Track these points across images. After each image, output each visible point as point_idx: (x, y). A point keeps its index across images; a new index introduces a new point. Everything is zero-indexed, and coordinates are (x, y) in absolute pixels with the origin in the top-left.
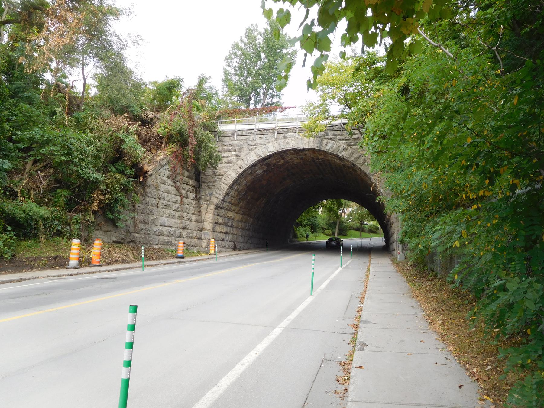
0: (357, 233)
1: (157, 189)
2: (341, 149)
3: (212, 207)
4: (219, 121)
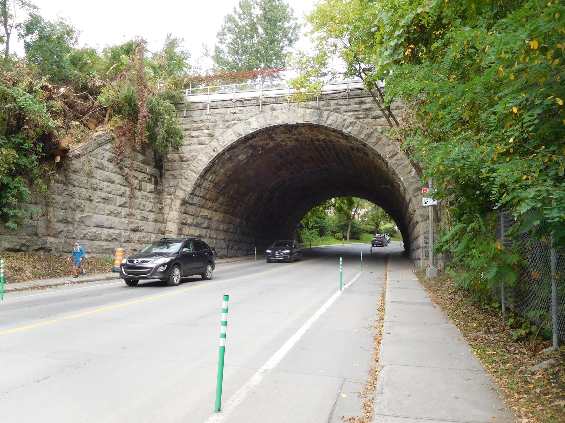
1: (90, 175)
2: (347, 123)
3: (178, 203)
4: (187, 90)
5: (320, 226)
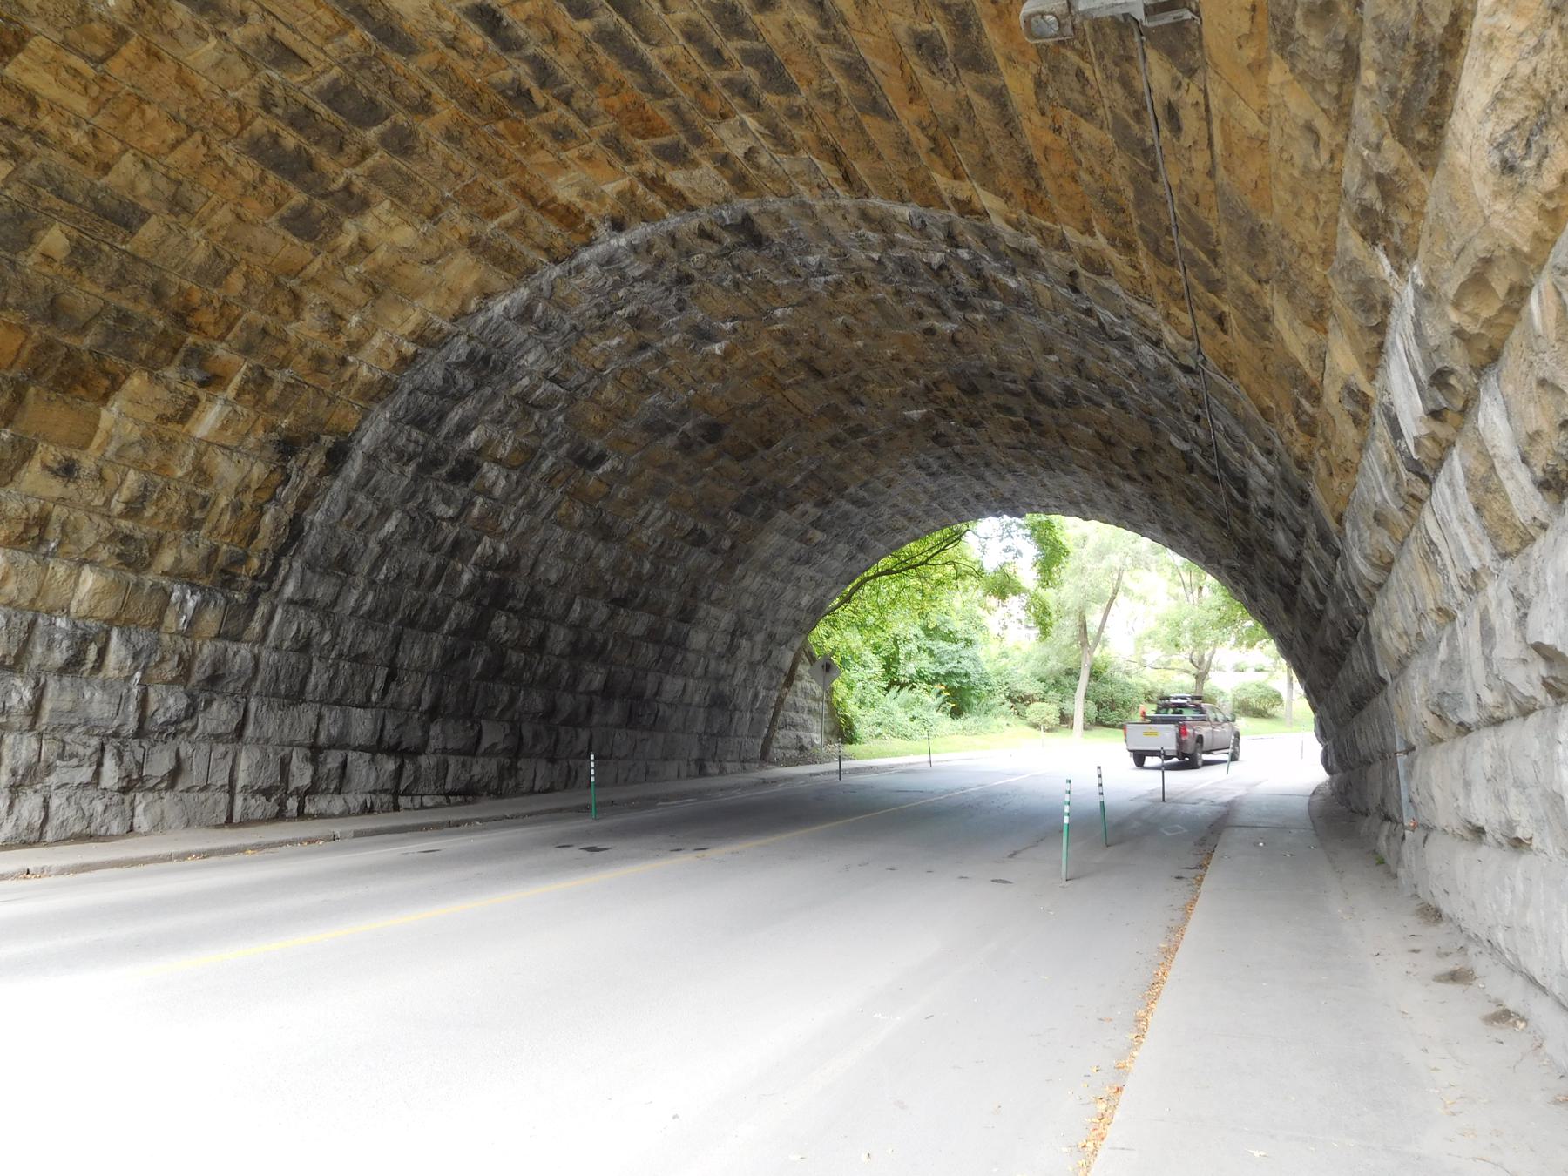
5: (950, 674)
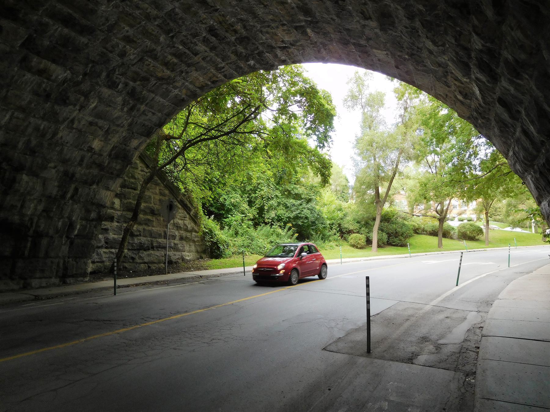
0: (434, 240)
5: (297, 218)
